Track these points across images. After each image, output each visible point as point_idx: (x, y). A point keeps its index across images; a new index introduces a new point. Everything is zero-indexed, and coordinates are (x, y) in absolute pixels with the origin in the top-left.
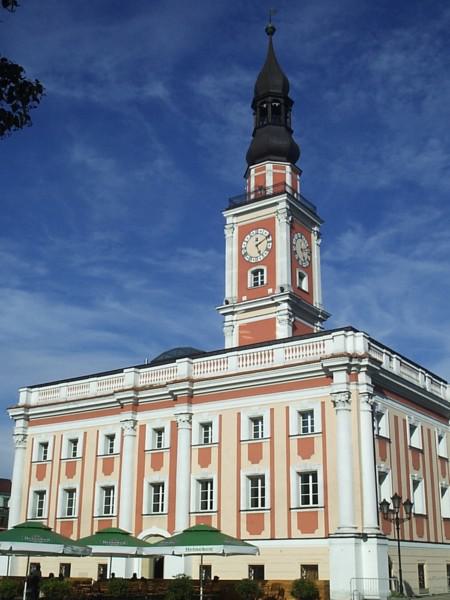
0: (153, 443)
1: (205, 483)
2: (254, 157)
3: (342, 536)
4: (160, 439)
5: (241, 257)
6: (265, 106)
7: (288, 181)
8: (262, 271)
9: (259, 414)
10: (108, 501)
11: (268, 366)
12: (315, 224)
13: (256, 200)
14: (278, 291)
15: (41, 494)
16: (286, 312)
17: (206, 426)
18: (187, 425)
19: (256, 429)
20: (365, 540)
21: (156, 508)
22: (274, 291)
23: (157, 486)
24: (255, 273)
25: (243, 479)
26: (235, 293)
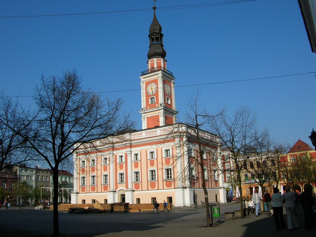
0: (120, 160)
1: (137, 173)
2: (150, 56)
3: (178, 188)
4: (122, 159)
5: (147, 93)
6: (153, 37)
7: (162, 66)
8: (154, 98)
9: (153, 151)
10: (106, 179)
11: (155, 135)
12: (172, 79)
13: (151, 72)
14: (159, 105)
15: (84, 178)
16: (163, 113)
17: (136, 155)
18: (130, 155)
19: (152, 155)
20: (186, 189)
21: (122, 181)
22: (158, 105)
23: (121, 174)
24: (152, 99)
25: (149, 171)
26: (145, 106)
